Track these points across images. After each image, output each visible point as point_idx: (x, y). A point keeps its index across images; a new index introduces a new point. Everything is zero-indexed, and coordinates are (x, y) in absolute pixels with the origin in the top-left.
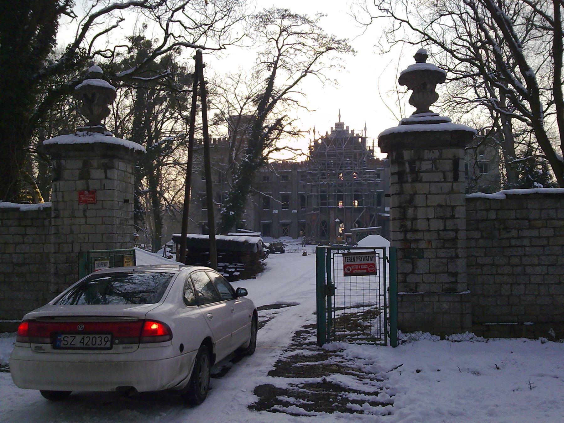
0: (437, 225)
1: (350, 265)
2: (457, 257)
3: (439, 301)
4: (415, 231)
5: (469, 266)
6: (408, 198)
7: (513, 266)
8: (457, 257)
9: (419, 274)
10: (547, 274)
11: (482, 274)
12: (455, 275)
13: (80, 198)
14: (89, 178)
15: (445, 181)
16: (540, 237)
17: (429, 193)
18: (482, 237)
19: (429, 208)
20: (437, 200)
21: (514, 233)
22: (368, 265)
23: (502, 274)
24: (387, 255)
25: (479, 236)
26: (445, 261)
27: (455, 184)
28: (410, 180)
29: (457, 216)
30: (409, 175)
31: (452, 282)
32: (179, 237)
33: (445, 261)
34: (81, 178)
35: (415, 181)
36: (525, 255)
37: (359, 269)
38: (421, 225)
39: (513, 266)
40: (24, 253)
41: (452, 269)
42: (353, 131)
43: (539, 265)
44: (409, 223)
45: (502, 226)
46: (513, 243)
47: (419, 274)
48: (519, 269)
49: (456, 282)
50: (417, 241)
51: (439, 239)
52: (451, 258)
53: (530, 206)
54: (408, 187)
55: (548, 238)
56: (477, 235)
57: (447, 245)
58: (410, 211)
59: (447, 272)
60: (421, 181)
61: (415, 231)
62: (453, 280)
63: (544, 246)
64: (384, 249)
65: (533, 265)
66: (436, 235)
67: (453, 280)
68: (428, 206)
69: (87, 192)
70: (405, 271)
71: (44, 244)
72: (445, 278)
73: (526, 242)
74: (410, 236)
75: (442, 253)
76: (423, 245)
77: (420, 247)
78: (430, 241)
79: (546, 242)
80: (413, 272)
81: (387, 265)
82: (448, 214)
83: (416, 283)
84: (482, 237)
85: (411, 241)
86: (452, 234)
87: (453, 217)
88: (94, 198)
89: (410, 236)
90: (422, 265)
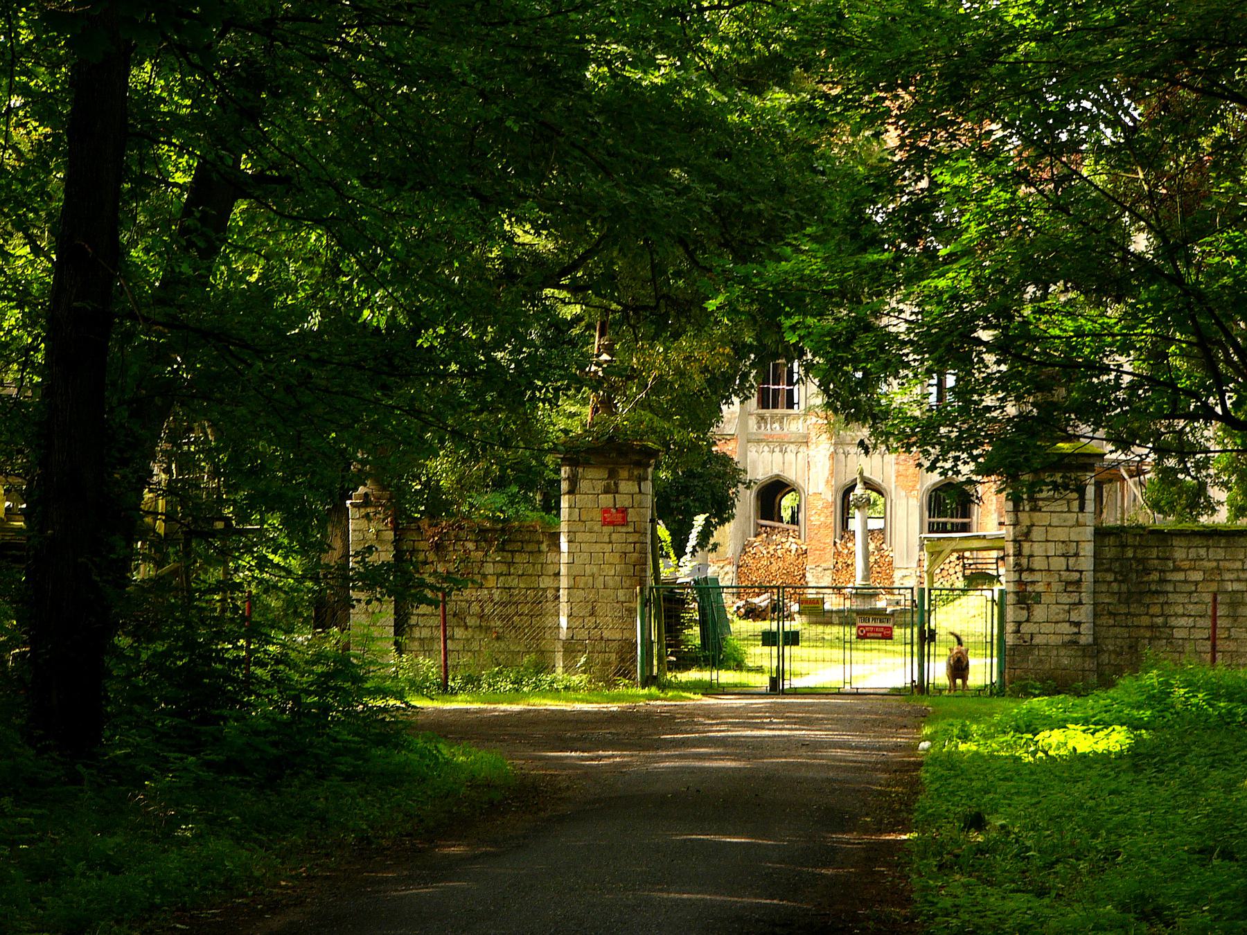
0: (1058, 563)
1: (864, 627)
2: (1080, 603)
3: (1057, 656)
4: (1031, 570)
5: (1095, 615)
6: (1025, 530)
7: (1152, 616)
8: (1080, 603)
9: (1036, 623)
10: (1194, 627)
11: (1114, 626)
12: (1078, 624)
13: (605, 518)
14: (617, 492)
15: (1069, 511)
16: (1186, 581)
17: (1050, 525)
18: (1115, 580)
19: (1049, 544)
20: (1061, 534)
21: (1155, 576)
22: (885, 628)
23: (1138, 626)
24: (996, 598)
25: (1112, 579)
26: (1067, 607)
27: (1080, 515)
28: (1027, 508)
29: (1082, 554)
30: (1026, 502)
31: (1075, 634)
32: (20, 528)
33: (1067, 607)
34: (606, 492)
35: (1034, 509)
36: (1166, 603)
37: (873, 632)
38: (1038, 563)
39: (1152, 616)
40: (510, 588)
41: (1074, 618)
42: (999, 491)
43: (1184, 615)
44: (1024, 561)
45: (1141, 567)
46: (1153, 587)
47: (1036, 623)
48: (1160, 620)
49: (1079, 633)
50: (1033, 583)
51: (1060, 581)
52: (1075, 604)
53: (1175, 543)
54: (1025, 518)
55: (1196, 583)
56: (1110, 577)
57: (1069, 589)
58: (1026, 546)
59: (1069, 621)
60: (1040, 510)
61: (1031, 570)
62: (1076, 630)
63: (1191, 593)
64: (912, 589)
65: (1176, 615)
66: (1057, 576)
67: (1076, 630)
68: (1047, 541)
69: (613, 511)
70: (1018, 620)
71: (539, 576)
72: (1066, 628)
73: (1170, 588)
74: (1026, 577)
75: (1064, 598)
76: (1040, 588)
77: (1037, 590)
78: (1049, 584)
79: (1193, 588)
80: (1028, 621)
81: (996, 608)
82: (1072, 552)
83: (1032, 634)
84: (1115, 580)
85: (1026, 584)
86: (1076, 576)
87: (1076, 555)
88: (624, 518)
89: (1026, 577)
90: (1039, 612)
